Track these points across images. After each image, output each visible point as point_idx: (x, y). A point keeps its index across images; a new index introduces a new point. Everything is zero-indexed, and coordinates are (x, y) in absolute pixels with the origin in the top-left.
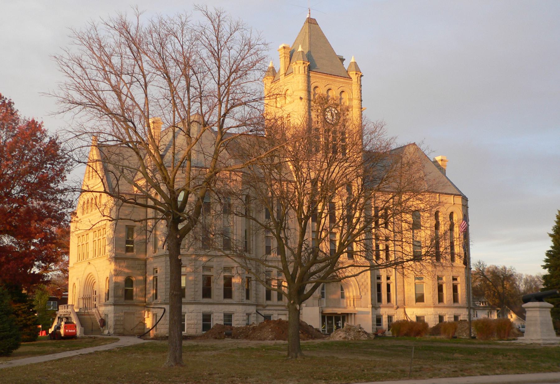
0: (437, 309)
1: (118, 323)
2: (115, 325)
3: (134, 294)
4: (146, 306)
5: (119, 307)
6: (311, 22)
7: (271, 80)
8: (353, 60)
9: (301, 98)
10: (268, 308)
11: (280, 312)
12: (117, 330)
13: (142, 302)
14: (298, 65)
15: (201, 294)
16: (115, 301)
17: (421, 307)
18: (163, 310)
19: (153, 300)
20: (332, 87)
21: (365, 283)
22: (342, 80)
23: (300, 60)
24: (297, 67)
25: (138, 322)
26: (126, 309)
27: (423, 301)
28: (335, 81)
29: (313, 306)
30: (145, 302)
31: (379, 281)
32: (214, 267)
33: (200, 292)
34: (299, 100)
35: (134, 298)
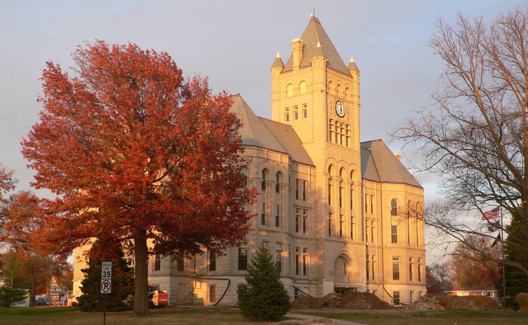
0: (409, 286)
1: (174, 293)
2: (171, 295)
3: (185, 265)
4: (199, 277)
5: (174, 278)
6: (315, 20)
7: (280, 70)
8: (278, 56)
9: (322, 91)
10: (297, 281)
11: (305, 285)
12: (173, 300)
13: (192, 273)
14: (319, 60)
15: (237, 266)
16: (171, 272)
17: (398, 284)
18: (227, 282)
19: (207, 271)
20: (341, 83)
21: (362, 262)
22: (347, 78)
23: (321, 55)
24: (317, 61)
25: (188, 293)
26: (179, 280)
27: (398, 279)
28: (343, 78)
29: (330, 281)
30: (195, 273)
31: (297, 253)
32: (270, 242)
33: (236, 264)
34: (320, 92)
35: (185, 269)
